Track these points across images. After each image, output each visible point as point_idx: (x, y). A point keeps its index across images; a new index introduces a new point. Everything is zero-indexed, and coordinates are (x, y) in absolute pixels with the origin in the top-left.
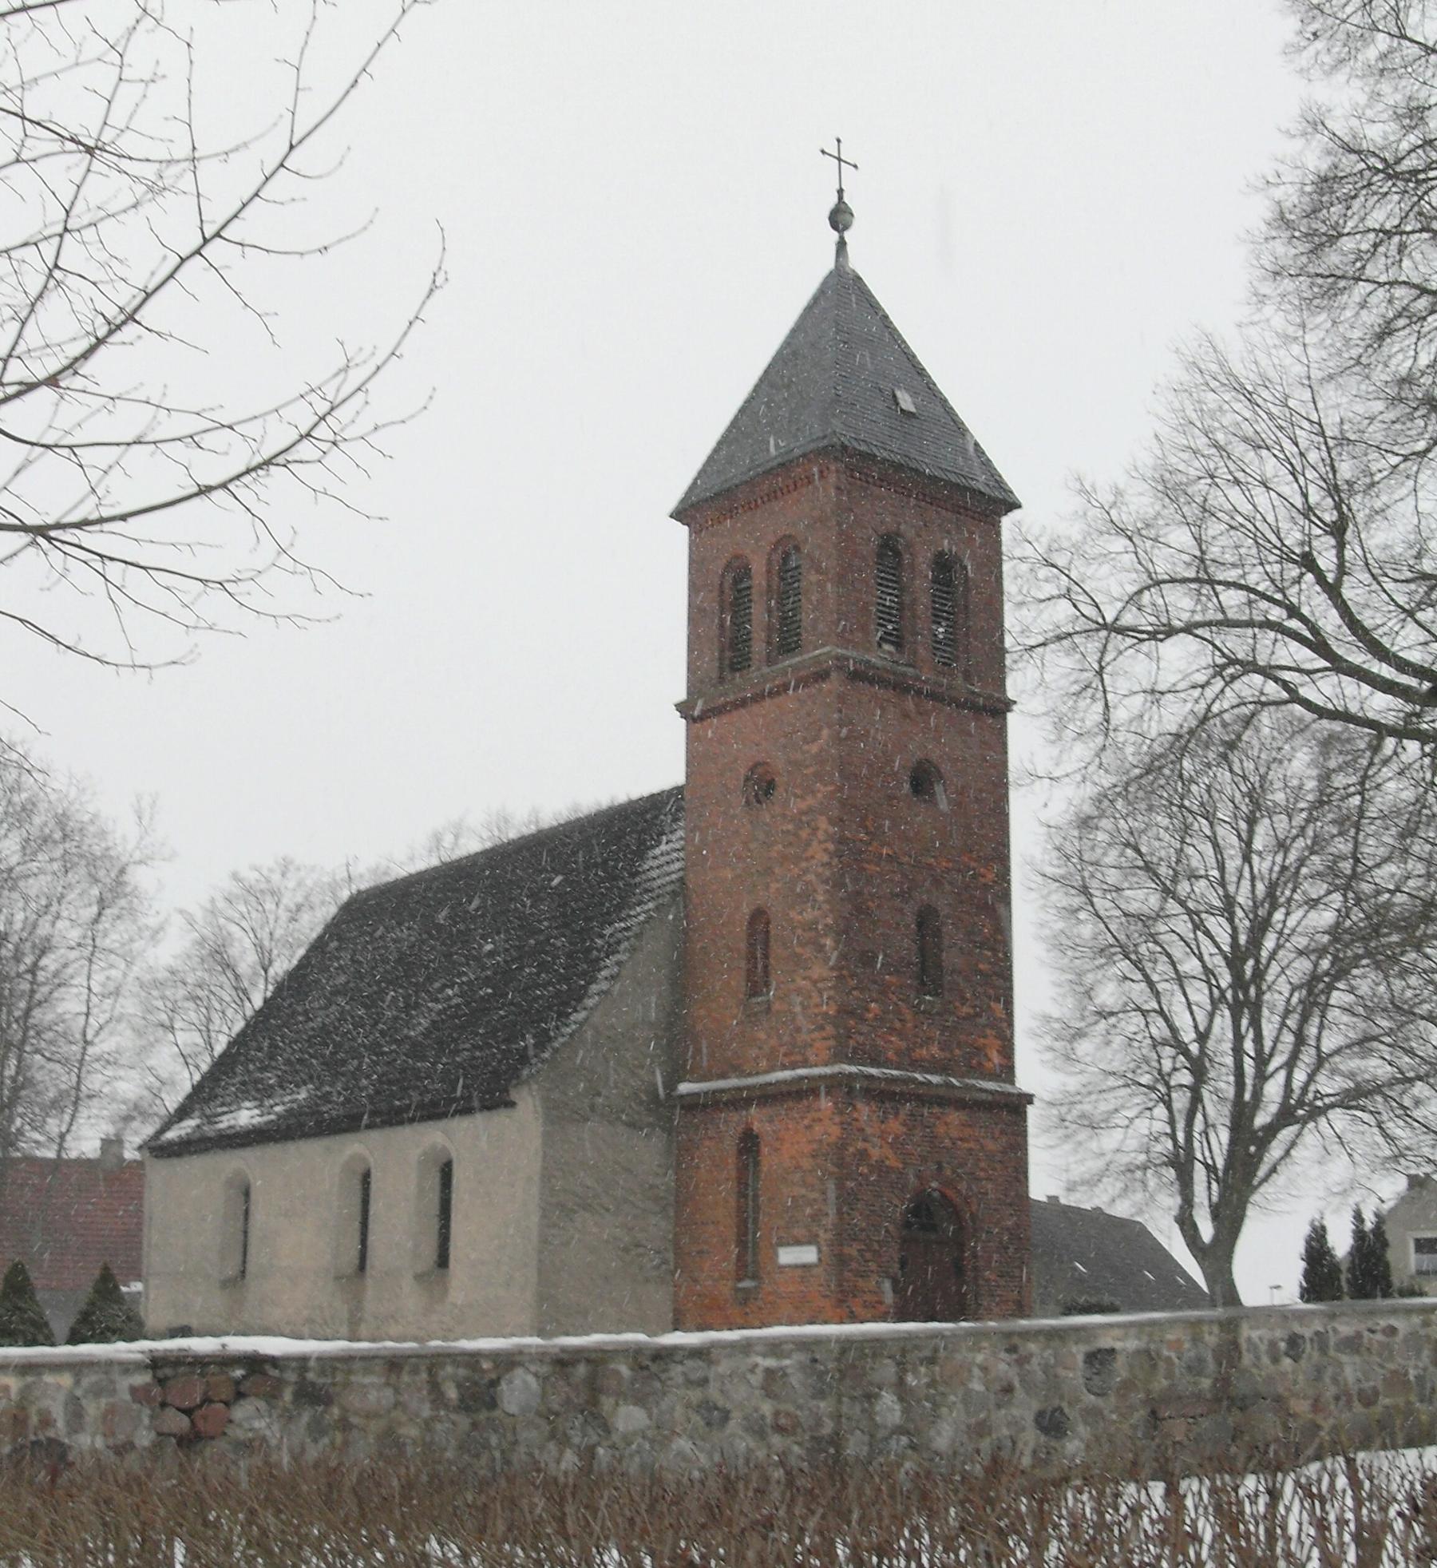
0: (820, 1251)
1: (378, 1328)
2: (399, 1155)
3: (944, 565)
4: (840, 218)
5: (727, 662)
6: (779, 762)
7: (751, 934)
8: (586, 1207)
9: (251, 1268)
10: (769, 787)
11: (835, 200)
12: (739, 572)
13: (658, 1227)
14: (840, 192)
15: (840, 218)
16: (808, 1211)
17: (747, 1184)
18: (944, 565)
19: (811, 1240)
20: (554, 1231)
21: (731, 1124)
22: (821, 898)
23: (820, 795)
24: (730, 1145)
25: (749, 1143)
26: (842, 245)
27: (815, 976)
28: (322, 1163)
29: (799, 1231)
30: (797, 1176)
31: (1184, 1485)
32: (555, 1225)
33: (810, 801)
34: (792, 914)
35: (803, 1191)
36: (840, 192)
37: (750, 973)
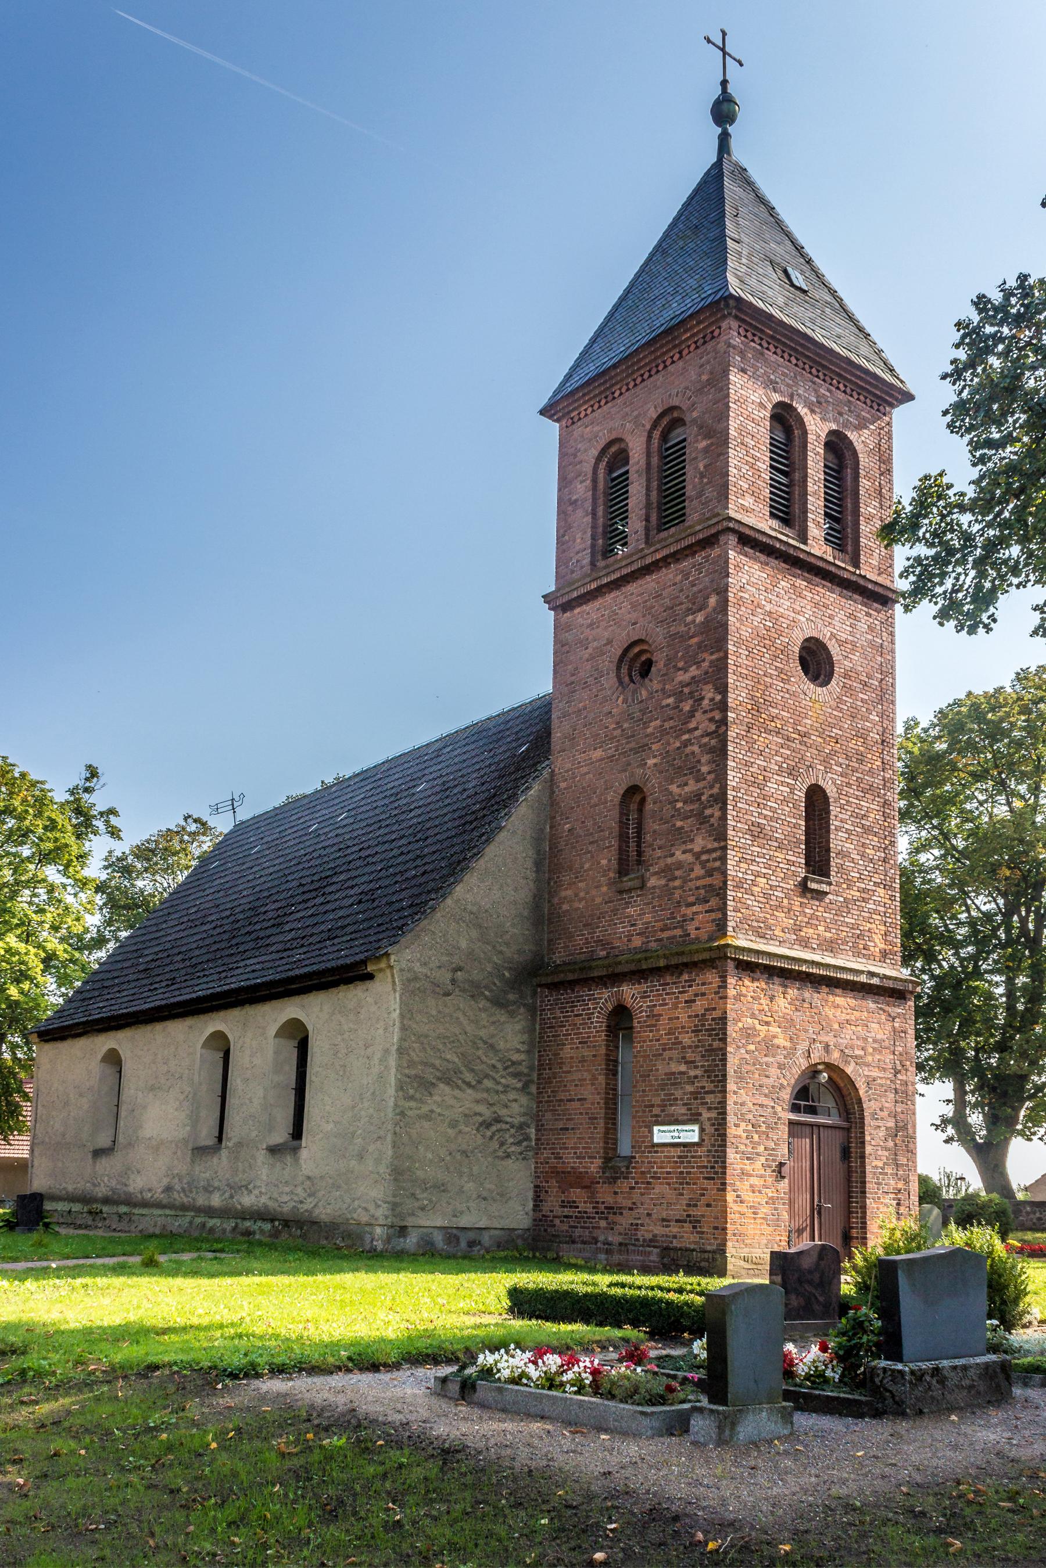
0: (702, 1130)
1: (232, 1197)
2: (255, 1036)
3: (838, 447)
4: (723, 111)
5: (600, 530)
6: (658, 635)
7: (624, 813)
8: (448, 1082)
9: (121, 1139)
10: (646, 669)
11: (719, 91)
12: (615, 456)
13: (516, 1107)
14: (724, 83)
15: (723, 111)
16: (690, 1088)
17: (616, 1061)
18: (838, 447)
19: (693, 1118)
20: (413, 1104)
21: (604, 998)
22: (705, 769)
23: (706, 664)
24: (598, 1023)
25: (620, 1019)
26: (724, 140)
27: (697, 849)
28: (183, 1042)
29: (680, 1110)
30: (675, 1054)
31: (656, 1140)
32: (412, 1098)
33: (693, 671)
34: (674, 788)
35: (683, 1068)
36: (724, 83)
37: (622, 852)
